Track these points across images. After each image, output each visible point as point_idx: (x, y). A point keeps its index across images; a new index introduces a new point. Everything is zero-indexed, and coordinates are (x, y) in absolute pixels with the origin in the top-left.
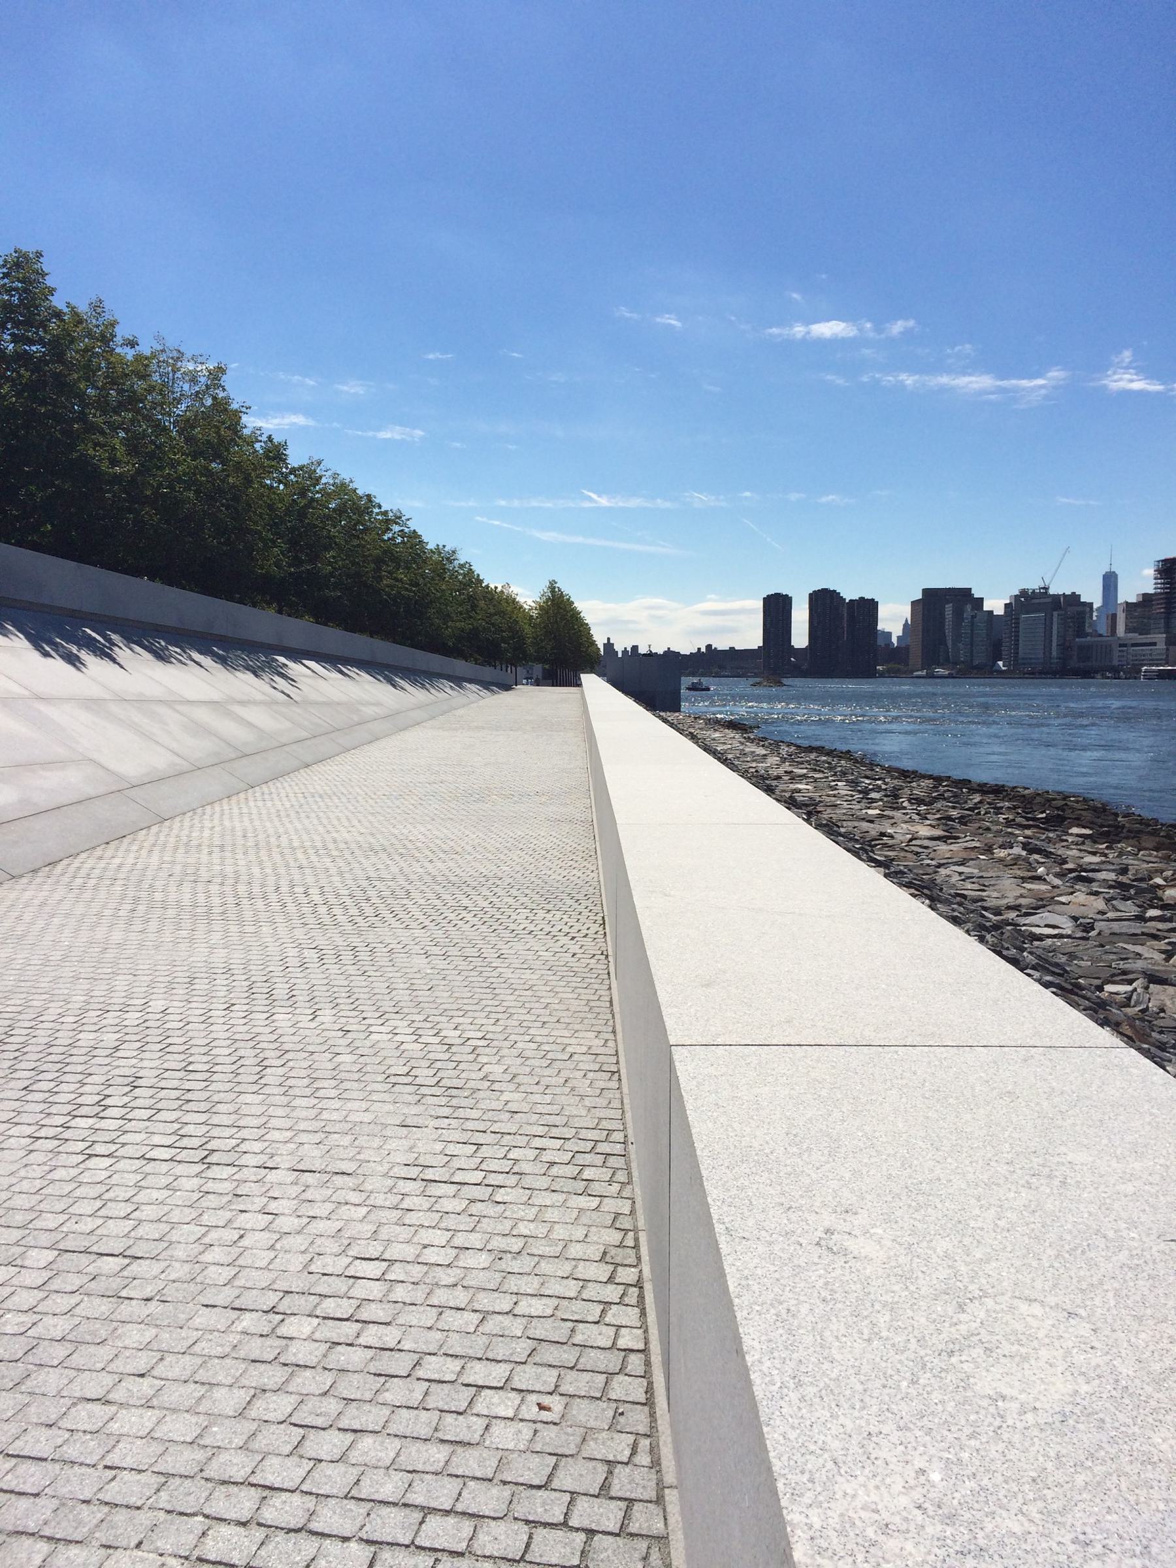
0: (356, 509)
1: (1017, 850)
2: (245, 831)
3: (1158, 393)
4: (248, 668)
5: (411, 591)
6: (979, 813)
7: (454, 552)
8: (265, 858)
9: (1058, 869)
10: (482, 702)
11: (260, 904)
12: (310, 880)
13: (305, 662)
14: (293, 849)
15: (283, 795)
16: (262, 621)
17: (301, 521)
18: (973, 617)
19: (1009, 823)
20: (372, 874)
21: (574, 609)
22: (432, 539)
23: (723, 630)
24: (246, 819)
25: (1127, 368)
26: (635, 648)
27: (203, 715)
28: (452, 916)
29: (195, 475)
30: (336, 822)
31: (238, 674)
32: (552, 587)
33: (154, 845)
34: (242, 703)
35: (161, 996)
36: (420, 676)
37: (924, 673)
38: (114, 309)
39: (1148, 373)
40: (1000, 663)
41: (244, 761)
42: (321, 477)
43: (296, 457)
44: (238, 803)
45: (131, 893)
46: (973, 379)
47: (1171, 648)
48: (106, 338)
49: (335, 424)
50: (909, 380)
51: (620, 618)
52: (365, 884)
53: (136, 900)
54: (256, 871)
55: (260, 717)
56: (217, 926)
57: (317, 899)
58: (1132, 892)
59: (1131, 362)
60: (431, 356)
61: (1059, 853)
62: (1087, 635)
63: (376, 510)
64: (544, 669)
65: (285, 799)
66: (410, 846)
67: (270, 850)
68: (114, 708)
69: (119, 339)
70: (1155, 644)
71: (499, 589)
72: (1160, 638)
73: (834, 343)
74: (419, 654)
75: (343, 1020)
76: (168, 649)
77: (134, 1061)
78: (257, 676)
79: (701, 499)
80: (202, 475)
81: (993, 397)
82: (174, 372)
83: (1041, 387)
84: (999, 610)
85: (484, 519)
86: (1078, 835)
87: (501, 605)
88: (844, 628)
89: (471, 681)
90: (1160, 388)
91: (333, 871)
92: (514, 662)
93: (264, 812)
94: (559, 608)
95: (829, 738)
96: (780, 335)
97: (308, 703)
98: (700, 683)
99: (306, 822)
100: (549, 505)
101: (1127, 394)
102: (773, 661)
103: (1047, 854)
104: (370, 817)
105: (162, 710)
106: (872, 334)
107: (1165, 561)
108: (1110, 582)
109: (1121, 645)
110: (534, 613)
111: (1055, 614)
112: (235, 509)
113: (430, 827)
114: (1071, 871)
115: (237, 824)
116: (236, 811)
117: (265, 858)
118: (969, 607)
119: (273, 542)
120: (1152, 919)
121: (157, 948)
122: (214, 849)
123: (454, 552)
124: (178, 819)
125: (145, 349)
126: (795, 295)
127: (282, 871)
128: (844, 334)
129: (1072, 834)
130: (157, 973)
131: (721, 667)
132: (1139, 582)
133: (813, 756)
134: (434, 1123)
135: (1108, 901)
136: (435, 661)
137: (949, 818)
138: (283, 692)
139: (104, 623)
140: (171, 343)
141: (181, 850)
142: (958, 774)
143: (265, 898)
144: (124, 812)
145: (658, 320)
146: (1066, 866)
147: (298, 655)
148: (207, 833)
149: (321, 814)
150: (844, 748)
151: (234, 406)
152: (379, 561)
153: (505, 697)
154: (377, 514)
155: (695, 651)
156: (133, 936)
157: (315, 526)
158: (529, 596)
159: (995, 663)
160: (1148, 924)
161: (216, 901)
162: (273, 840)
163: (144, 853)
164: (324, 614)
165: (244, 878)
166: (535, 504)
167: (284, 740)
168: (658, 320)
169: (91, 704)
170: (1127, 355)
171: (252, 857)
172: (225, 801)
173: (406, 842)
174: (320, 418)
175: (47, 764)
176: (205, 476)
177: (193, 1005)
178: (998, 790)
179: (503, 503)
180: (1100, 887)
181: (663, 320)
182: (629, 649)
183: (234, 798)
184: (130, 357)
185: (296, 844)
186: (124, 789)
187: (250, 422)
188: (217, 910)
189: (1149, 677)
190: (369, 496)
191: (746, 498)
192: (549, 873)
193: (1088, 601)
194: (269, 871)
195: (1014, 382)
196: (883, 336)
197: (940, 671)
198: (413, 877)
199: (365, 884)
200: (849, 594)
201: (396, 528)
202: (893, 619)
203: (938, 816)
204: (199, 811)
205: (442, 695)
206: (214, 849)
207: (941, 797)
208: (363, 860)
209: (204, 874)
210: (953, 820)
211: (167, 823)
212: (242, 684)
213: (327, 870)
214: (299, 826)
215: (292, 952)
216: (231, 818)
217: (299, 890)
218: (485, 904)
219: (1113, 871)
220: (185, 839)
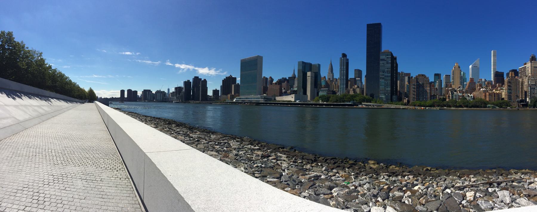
0: (62, 76)
16: (47, 93)
21: (81, 89)
27: (36, 108)
36: (71, 101)
38: (25, 42)
43: (53, 68)
48: (23, 47)
51: (100, 93)
52: (64, 149)
55: (46, 108)
57: (54, 154)
68: (20, 107)
73: (129, 55)
79: (110, 76)
87: (83, 91)
88: (132, 95)
91: (57, 144)
92: (84, 99)
95: (131, 110)
97: (54, 106)
102: (122, 99)
105: (29, 107)
108: (169, 90)
132: (172, 90)
136: (73, 99)
139: (21, 92)
140: (34, 49)
144: (20, 127)
147: (52, 98)
152: (65, 84)
158: (87, 90)
164: (57, 92)
169: (16, 106)
174: (57, 63)
175: (4, 118)
178: (159, 119)
186: (19, 123)
198: (75, 147)
199: (64, 149)
200: (133, 90)
202: (139, 94)
212: (43, 103)
217: (50, 151)
218: (92, 157)
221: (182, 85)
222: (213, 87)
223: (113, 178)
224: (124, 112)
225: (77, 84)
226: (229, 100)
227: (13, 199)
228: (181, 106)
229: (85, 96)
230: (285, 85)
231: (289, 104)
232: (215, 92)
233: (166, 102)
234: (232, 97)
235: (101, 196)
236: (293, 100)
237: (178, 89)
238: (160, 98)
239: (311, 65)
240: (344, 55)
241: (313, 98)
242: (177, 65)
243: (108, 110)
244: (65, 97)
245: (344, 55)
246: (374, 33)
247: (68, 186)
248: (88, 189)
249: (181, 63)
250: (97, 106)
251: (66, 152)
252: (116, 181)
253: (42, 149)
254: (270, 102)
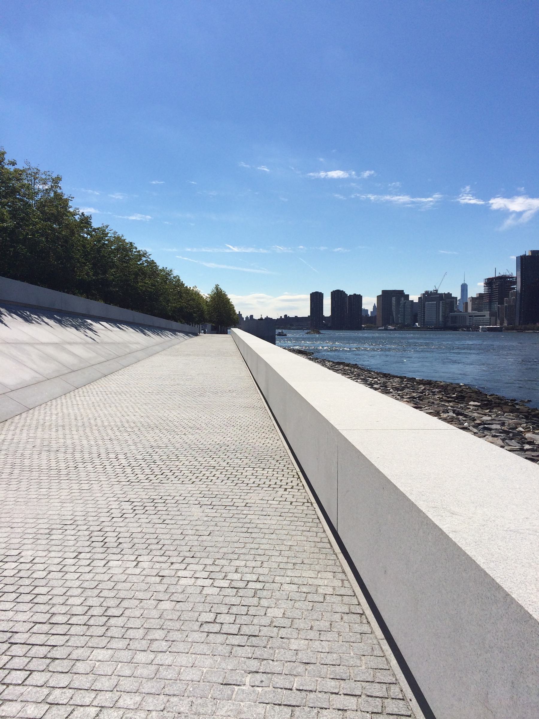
0: (124, 249)
1: (451, 414)
2: (75, 416)
3: (482, 205)
4: (73, 326)
5: (152, 288)
6: (425, 395)
7: (171, 271)
8: (89, 434)
9: (473, 424)
10: (186, 342)
11: (90, 467)
12: (118, 449)
13: (13, 314)
14: (105, 427)
15: (95, 393)
16: (78, 302)
17: (98, 254)
18: (405, 303)
19: (441, 399)
20: (154, 444)
22: (161, 264)
23: (291, 308)
24: (75, 408)
25: (468, 194)
26: (252, 316)
27: (51, 350)
28: (208, 474)
29: (45, 229)
30: (126, 410)
31: (68, 329)
32: (217, 288)
33: (24, 426)
34: (70, 343)
35: (29, 547)
36: (157, 329)
37: (383, 328)
39: (476, 195)
40: (417, 324)
41: (73, 374)
42: (108, 233)
43: (95, 224)
44: (70, 398)
45: (10, 460)
46: (401, 197)
47: (492, 318)
49: (109, 213)
50: (372, 197)
51: (247, 303)
52: (150, 450)
53: (13, 465)
54: (85, 442)
55: (79, 350)
56: (65, 484)
57: (124, 462)
58: (511, 435)
59: (470, 191)
60: (154, 182)
61: (470, 415)
62: (455, 312)
63: (134, 250)
64: (212, 326)
65: (96, 395)
66: (170, 424)
67: (91, 428)
69: (6, 161)
70: (485, 316)
71: (191, 289)
72: (487, 313)
73: (339, 180)
74: (155, 318)
75: (158, 566)
76: (31, 316)
77: (11, 614)
78: (77, 330)
79: (280, 249)
80: (49, 230)
81: (409, 206)
82: (35, 179)
83: (431, 201)
84: (416, 300)
85: (181, 257)
86: (474, 405)
89: (180, 332)
90: (482, 203)
91: (130, 442)
92: (198, 323)
93: (85, 403)
94: (220, 297)
96: (314, 176)
97: (103, 343)
98: (282, 332)
99: (109, 409)
100: (209, 251)
101: (467, 205)
102: (314, 322)
103: (466, 416)
104: (145, 406)
105: (27, 348)
106: (355, 177)
107: (488, 279)
108: (464, 288)
109: (470, 316)
110: (208, 300)
111: (441, 302)
112: (66, 247)
113: (178, 412)
114: (479, 424)
115: (71, 411)
116: (69, 403)
117: (89, 434)
118: (403, 299)
119: (84, 263)
120: (528, 450)
121: (26, 503)
122: (59, 428)
123: (171, 271)
124: (37, 408)
125: (20, 166)
126: (321, 159)
127: (100, 442)
128: (342, 176)
129: (470, 405)
130: (27, 526)
131: (292, 325)
132: (477, 288)
133: (342, 367)
134: (248, 679)
135: (503, 440)
137: (414, 397)
138: (91, 338)
140: (33, 165)
141: (40, 429)
142: (410, 375)
143: (92, 462)
145: (259, 168)
146: (476, 422)
147: (97, 319)
148: (54, 417)
149: (117, 405)
150: (354, 363)
151: (65, 197)
152: (136, 275)
153: (195, 339)
154: (135, 252)
155: (279, 318)
156: (11, 494)
157: (105, 257)
159: (414, 324)
160: (527, 453)
161: (63, 465)
162: (92, 421)
163: (18, 431)
164: (109, 299)
165: (78, 448)
166: (204, 250)
167: (93, 363)
168: (259, 168)
170: (468, 188)
171: (81, 433)
172: (63, 397)
173: (168, 422)
174: (108, 206)
176: (51, 230)
177: (53, 554)
178: (429, 383)
179: (189, 250)
180: (495, 432)
181: (261, 168)
182: (249, 317)
183: (68, 395)
184: (12, 170)
185: (106, 424)
187: (73, 206)
188: (64, 472)
189: (484, 330)
190: (131, 243)
191: (301, 249)
192: (254, 441)
193: (376, 299)
194: (92, 443)
195: (419, 199)
196: (360, 178)
197: (390, 327)
198: (177, 445)
199: (150, 450)
200: (349, 292)
201: (144, 259)
202: (369, 304)
203: (408, 396)
204: (49, 403)
205: (167, 339)
206: (59, 428)
207: (406, 387)
208: (147, 435)
209: (54, 446)
210: (416, 398)
211: (31, 411)
212: (70, 334)
213: (126, 441)
214: (106, 412)
215: (115, 505)
216: (67, 408)
217: (112, 456)
218: (225, 464)
219: (499, 424)
220: (41, 422)
223: (274, 502)
224: (322, 362)
225: (175, 273)
227: (47, 544)
229: (202, 312)
233: (455, 329)
235: (245, 530)
237: (497, 285)
238: (438, 315)
242: (497, 203)
243: (274, 355)
244: (138, 316)
245: (387, 714)
247: (170, 517)
248: (217, 519)
249: (510, 195)
250: (239, 343)
251: (156, 457)
252: (279, 506)
253: (90, 453)
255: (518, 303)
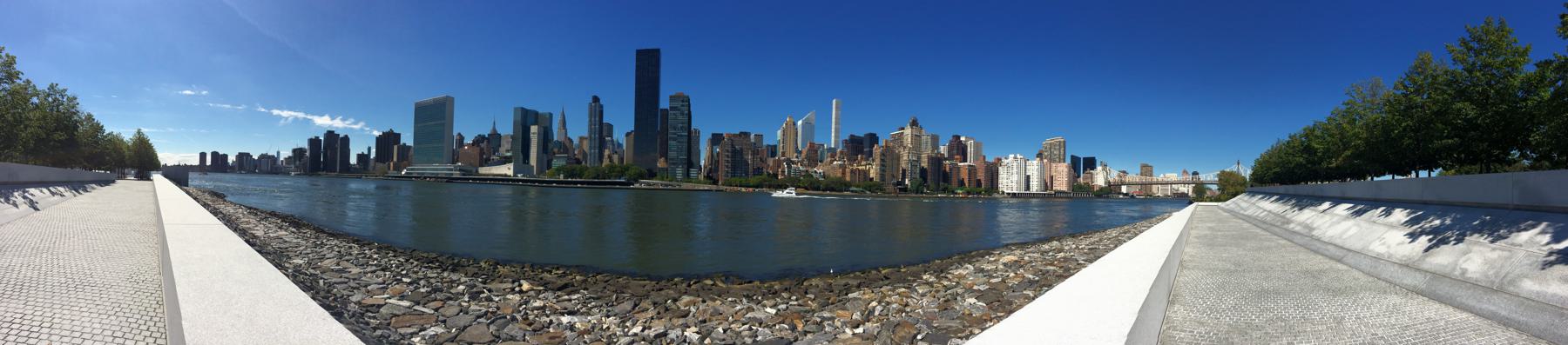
4: (1479, 230)
86: (360, 192)
87: (115, 141)
102: (202, 168)
132: (286, 153)
158: (128, 135)
202: (231, 159)
221: (305, 145)
222: (362, 144)
226: (392, 172)
228: (304, 182)
230: (488, 147)
231: (504, 180)
232: (361, 157)
234: (398, 168)
236: (511, 173)
237: (298, 152)
238: (268, 165)
239: (536, 113)
240: (596, 99)
241: (540, 171)
242: (276, 112)
245: (596, 99)
246: (648, 66)
249: (281, 109)
254: (469, 177)
255: (373, 151)
